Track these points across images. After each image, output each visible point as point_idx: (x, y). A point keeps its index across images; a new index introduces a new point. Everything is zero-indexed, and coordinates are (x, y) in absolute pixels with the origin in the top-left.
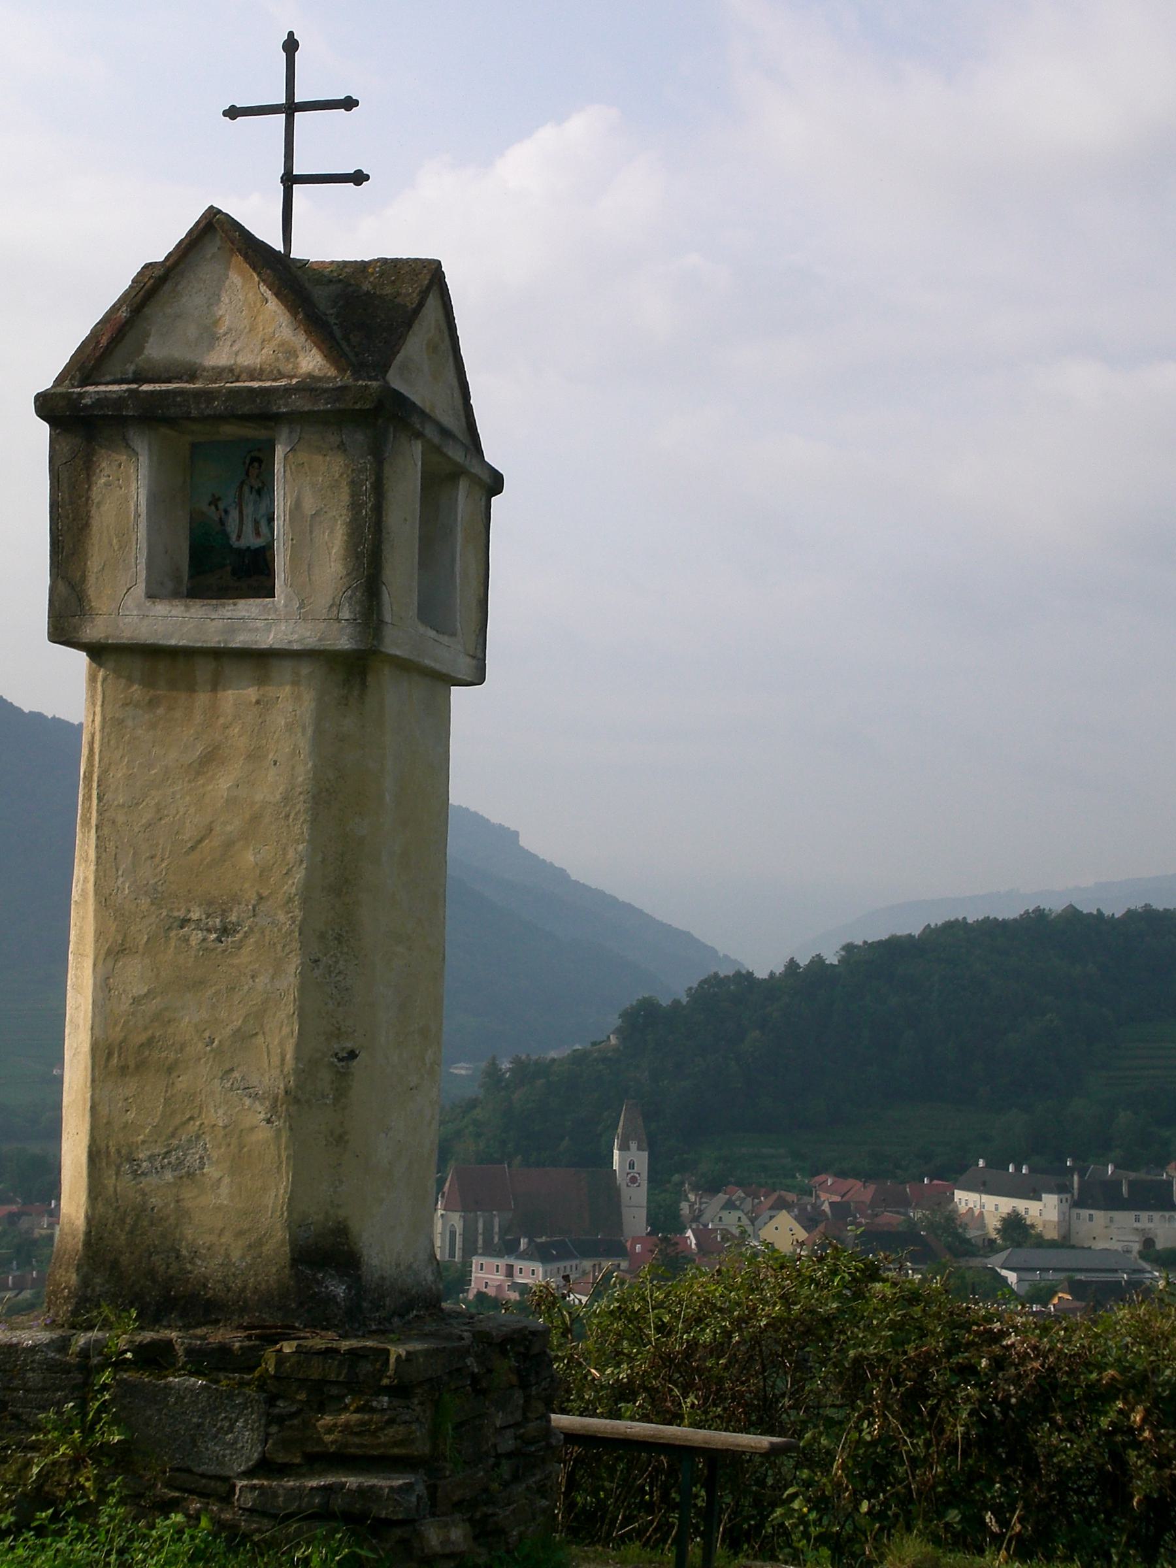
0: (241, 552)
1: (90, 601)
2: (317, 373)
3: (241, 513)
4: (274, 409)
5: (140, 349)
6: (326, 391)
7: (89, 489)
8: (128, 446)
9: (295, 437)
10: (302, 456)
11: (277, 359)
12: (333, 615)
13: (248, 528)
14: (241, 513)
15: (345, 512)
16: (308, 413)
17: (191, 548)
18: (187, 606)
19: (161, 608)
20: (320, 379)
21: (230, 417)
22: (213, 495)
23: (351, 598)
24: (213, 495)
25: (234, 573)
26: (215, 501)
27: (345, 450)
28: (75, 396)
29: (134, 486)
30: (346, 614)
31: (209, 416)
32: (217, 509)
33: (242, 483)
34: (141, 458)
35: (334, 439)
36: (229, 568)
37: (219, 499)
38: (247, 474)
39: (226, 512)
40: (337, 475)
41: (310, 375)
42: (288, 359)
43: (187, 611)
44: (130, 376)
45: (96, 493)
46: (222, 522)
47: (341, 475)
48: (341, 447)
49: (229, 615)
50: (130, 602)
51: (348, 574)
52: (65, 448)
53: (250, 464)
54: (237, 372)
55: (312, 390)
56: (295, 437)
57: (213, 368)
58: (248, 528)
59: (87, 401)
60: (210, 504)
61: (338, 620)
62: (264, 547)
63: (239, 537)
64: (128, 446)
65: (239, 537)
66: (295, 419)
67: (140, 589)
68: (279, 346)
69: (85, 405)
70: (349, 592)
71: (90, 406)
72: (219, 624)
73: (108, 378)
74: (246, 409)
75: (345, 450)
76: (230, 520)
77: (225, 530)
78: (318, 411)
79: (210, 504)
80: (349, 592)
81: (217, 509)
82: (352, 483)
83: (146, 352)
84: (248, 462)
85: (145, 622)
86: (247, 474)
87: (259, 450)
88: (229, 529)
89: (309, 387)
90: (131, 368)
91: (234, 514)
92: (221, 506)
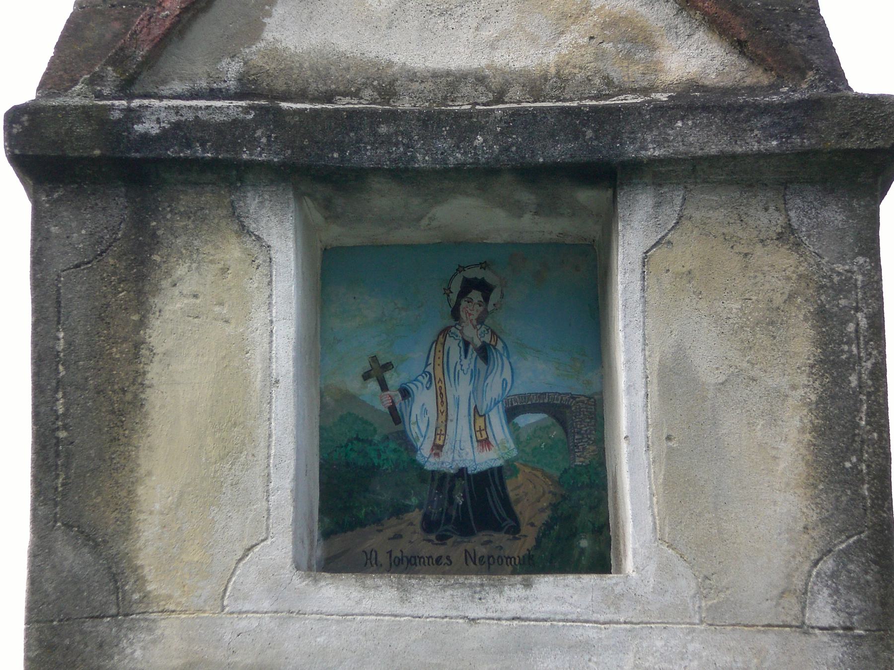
0: (443, 481)
1: (141, 580)
2: (712, 79)
3: (441, 396)
4: (631, 151)
5: (255, 30)
6: (768, 109)
7: (142, 323)
8: (243, 230)
9: (670, 215)
10: (687, 252)
11: (600, 56)
12: (790, 610)
13: (461, 430)
14: (441, 396)
15: (804, 379)
16: (713, 161)
17: (321, 467)
18: (402, 588)
19: (338, 593)
20: (733, 91)
21: (481, 176)
22: (374, 359)
23: (834, 575)
24: (374, 359)
25: (429, 525)
26: (377, 371)
27: (798, 244)
28: (116, 115)
29: (259, 317)
30: (823, 612)
31: (459, 168)
32: (384, 387)
33: (445, 332)
34: (277, 257)
35: (766, 218)
36: (416, 516)
37: (388, 366)
38: (455, 313)
39: (405, 393)
40: (778, 300)
41: (693, 85)
42: (629, 56)
43: (402, 601)
44: (232, 84)
45: (160, 334)
46: (396, 416)
47: (791, 297)
48: (787, 236)
49: (514, 608)
50: (247, 575)
51: (823, 521)
52: (78, 230)
53: (463, 294)
54: (496, 83)
55: (728, 109)
56: (670, 215)
57: (435, 75)
58: (461, 430)
59: (148, 127)
60: (366, 376)
61: (804, 628)
62: (500, 469)
63: (437, 448)
64: (243, 230)
65: (437, 448)
66: (662, 174)
67: (280, 547)
68: (605, 26)
69: (145, 137)
70: (828, 564)
71: (157, 138)
72: (486, 632)
73: (178, 87)
74: (560, 151)
75: (798, 244)
76: (416, 410)
77: (404, 432)
78: (745, 155)
79: (366, 376)
80: (828, 564)
81: (384, 387)
82: (822, 315)
83: (268, 35)
84: (456, 287)
85: (295, 627)
86: (455, 313)
87: (484, 265)
88: (414, 431)
89: (693, 101)
90: (232, 69)
91: (424, 399)
92: (393, 380)
